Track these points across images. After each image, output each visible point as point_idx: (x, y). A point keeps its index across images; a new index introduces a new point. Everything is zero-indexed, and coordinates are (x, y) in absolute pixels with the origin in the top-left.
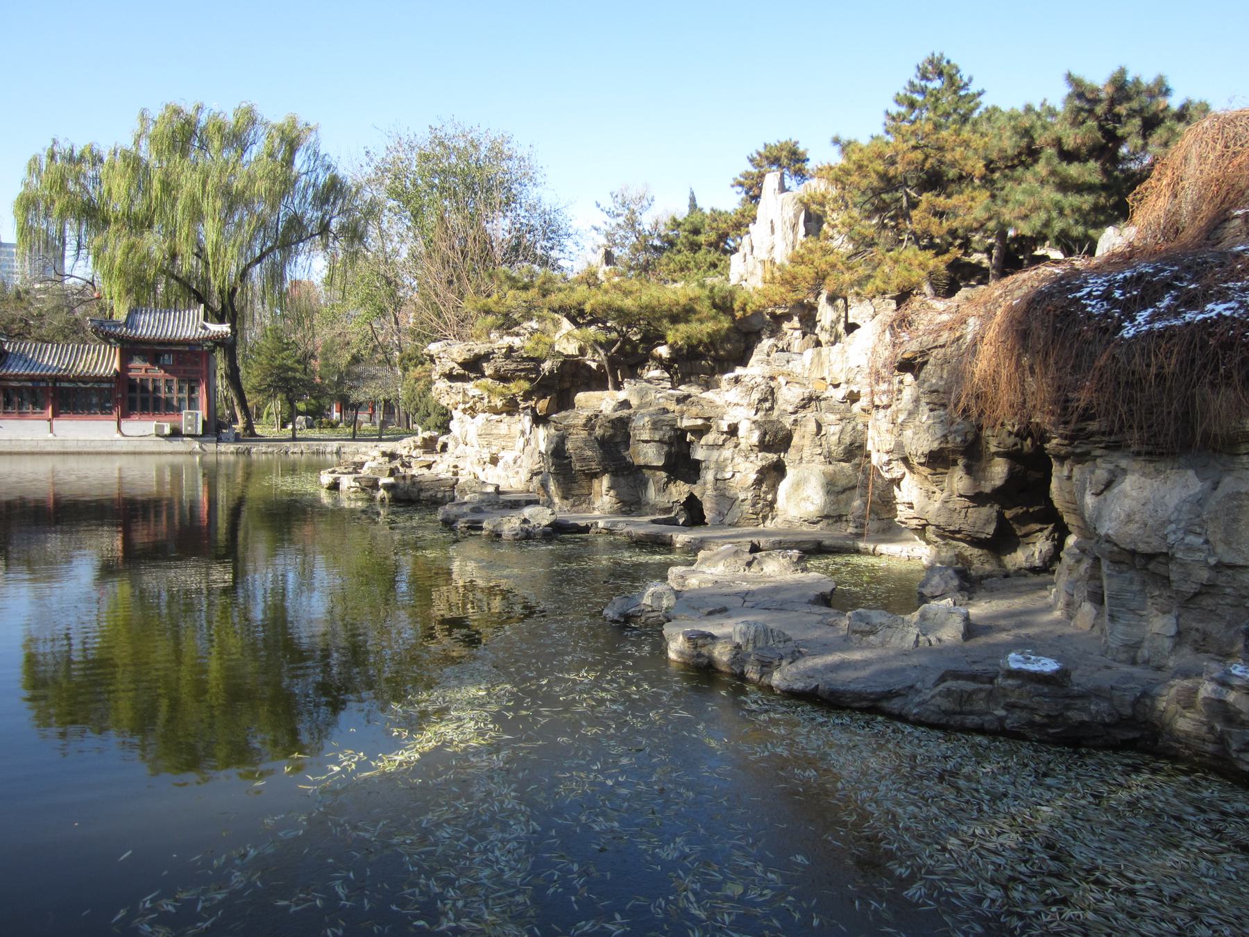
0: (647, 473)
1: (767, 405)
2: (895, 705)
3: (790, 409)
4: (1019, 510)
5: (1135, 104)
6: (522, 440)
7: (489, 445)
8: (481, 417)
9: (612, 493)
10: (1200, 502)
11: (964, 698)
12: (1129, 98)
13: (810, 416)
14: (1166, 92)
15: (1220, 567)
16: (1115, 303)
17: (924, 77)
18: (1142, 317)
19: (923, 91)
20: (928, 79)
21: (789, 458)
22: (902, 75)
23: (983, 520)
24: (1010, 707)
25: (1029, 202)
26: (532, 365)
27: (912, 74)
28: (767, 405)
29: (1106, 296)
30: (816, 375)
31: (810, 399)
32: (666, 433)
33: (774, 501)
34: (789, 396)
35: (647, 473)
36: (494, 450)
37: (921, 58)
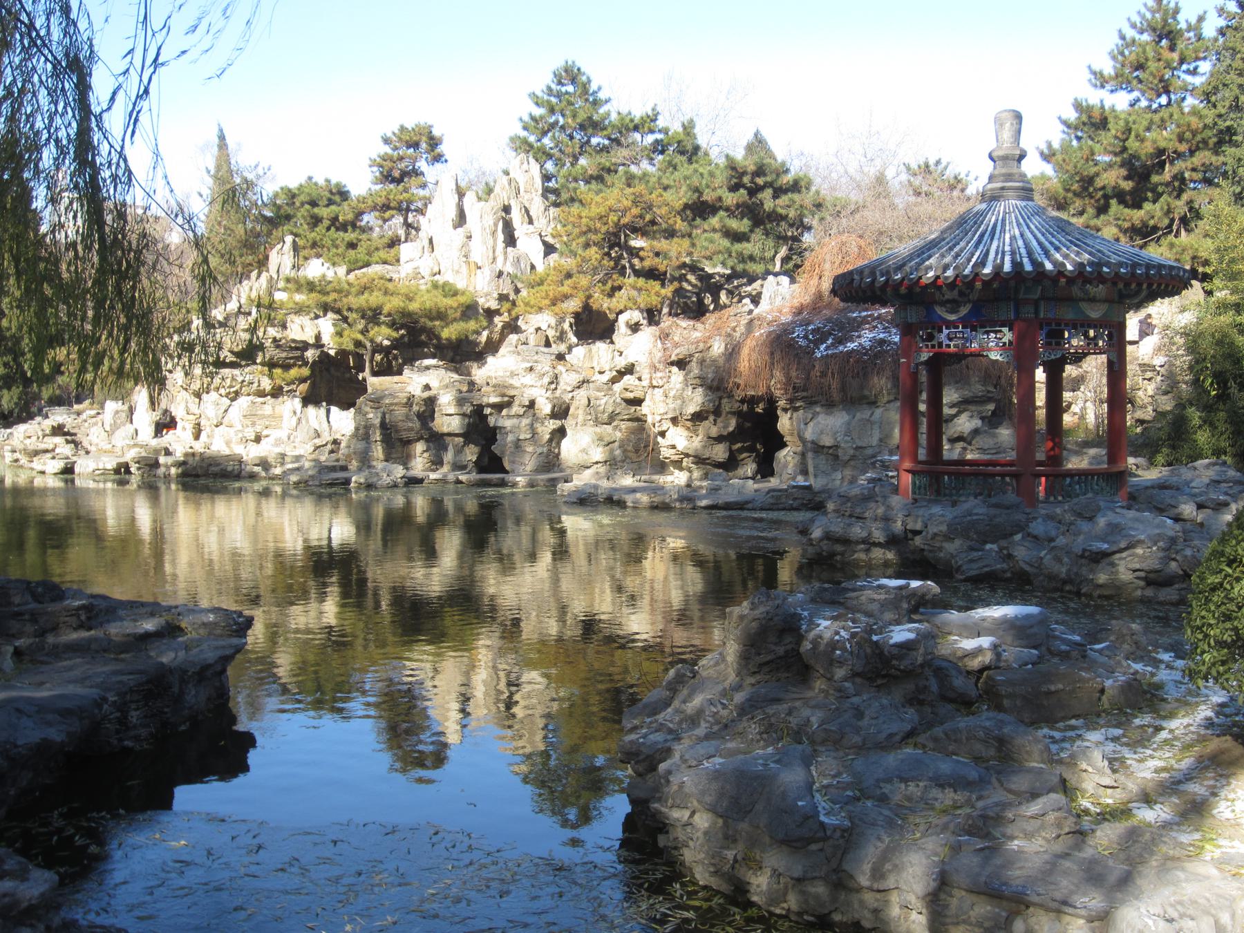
0: (448, 439)
1: (553, 386)
2: (750, 506)
3: (569, 389)
4: (739, 445)
5: (769, 179)
6: (295, 419)
7: (254, 424)
8: (243, 401)
9: (426, 455)
10: (849, 424)
11: (778, 498)
12: (765, 175)
13: (582, 395)
14: (787, 171)
15: (858, 448)
16: (810, 341)
17: (560, 83)
18: (823, 347)
19: (559, 95)
20: (563, 85)
21: (569, 423)
22: (542, 80)
23: (720, 452)
24: (795, 499)
25: (712, 247)
26: (298, 353)
27: (548, 79)
28: (553, 386)
29: (806, 337)
30: (587, 365)
31: (584, 382)
32: (468, 409)
33: (559, 454)
34: (568, 379)
35: (448, 439)
36: (258, 428)
37: (559, 64)
